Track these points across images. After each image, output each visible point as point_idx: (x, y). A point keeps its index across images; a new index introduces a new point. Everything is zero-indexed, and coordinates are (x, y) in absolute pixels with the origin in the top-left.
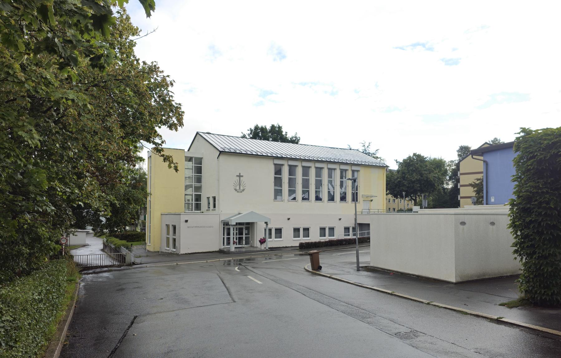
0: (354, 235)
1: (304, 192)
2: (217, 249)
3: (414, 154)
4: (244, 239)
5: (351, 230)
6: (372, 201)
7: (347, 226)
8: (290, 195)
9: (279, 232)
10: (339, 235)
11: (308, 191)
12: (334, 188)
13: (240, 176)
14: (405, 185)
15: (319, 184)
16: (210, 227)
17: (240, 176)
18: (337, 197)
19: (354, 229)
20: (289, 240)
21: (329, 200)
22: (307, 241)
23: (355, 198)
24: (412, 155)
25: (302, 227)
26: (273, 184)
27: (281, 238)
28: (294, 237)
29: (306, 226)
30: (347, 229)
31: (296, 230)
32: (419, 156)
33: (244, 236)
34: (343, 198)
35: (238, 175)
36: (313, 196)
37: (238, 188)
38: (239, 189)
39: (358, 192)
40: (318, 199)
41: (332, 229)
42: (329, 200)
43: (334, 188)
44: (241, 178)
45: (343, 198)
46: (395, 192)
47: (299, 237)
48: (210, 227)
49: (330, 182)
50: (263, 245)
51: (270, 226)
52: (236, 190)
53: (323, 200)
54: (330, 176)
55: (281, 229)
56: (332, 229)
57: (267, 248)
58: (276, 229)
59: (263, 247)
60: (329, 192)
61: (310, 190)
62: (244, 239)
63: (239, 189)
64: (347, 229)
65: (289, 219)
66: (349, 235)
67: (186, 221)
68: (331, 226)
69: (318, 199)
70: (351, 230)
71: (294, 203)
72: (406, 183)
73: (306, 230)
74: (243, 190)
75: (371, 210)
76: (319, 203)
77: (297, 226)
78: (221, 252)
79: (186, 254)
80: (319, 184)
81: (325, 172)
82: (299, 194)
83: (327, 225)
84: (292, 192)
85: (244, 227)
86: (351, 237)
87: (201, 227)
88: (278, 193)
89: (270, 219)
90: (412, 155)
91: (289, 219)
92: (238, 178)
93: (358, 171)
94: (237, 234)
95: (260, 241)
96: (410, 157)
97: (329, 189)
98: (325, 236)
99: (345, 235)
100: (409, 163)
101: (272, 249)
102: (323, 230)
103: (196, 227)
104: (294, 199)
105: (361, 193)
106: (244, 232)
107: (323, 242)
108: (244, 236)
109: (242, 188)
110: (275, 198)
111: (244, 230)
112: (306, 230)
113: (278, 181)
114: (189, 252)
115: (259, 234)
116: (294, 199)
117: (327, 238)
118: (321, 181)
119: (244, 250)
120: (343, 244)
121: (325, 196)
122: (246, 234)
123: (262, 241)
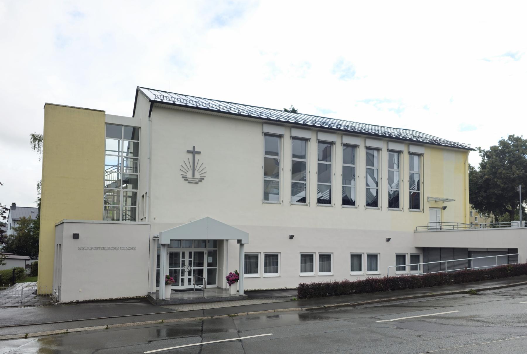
0: (413, 268)
1: (320, 189)
2: (142, 293)
3: (511, 137)
4: (205, 275)
5: (408, 259)
6: (445, 208)
7: (401, 251)
8: (294, 193)
9: (272, 261)
10: (387, 269)
11: (330, 188)
12: (377, 183)
13: (194, 152)
14: (499, 186)
15: (349, 174)
16: (129, 249)
17: (194, 152)
18: (384, 200)
19: (415, 258)
20: (290, 276)
21: (368, 205)
22: (374, 277)
23: (415, 203)
24: (497, 144)
25: (316, 252)
26: (262, 172)
27: (277, 272)
28: (302, 271)
29: (325, 251)
30: (400, 258)
31: (307, 260)
32: (518, 139)
33: (205, 268)
34: (394, 202)
35: (191, 149)
36: (337, 197)
37: (189, 175)
38: (193, 176)
39: (421, 192)
40: (347, 201)
41: (373, 258)
42: (368, 205)
43: (377, 183)
44: (197, 156)
45: (394, 202)
46: (480, 199)
47: (312, 271)
48: (129, 249)
49: (370, 172)
50: (233, 286)
51: (249, 249)
52: (185, 178)
53: (357, 204)
54: (370, 161)
55: (277, 255)
56: (373, 258)
57: (242, 293)
58: (267, 256)
59: (233, 290)
60: (368, 190)
61: (333, 184)
62: (205, 275)
63: (193, 176)
64: (400, 258)
65: (292, 237)
66: (404, 269)
67: (76, 236)
68: (373, 251)
69: (347, 201)
70: (408, 259)
71: (301, 207)
72: (499, 182)
73: (326, 258)
74: (201, 179)
75: (443, 224)
76: (348, 209)
77: (307, 251)
78: (148, 300)
79: (72, 303)
80: (349, 174)
81: (361, 155)
82: (312, 191)
83: (365, 250)
84: (297, 188)
85: (205, 250)
86: (408, 272)
87: (109, 249)
88: (270, 191)
89: (247, 235)
90: (497, 144)
91: (292, 237)
92: (190, 156)
93: (420, 155)
94: (183, 272)
95: (228, 278)
96: (502, 143)
97: (367, 185)
98: (360, 270)
99: (397, 269)
100: (502, 151)
101: (251, 294)
102: (356, 259)
103: (97, 248)
104: (303, 200)
105: (425, 195)
106: (206, 260)
107: (353, 284)
108: (205, 268)
109: (197, 176)
110: (266, 197)
111: (205, 257)
112: (326, 258)
113: (271, 169)
114: (80, 299)
115: (232, 262)
116: (303, 200)
117: (364, 274)
118: (353, 170)
119: (206, 295)
120: (399, 289)
121: (361, 199)
122: (209, 265)
123: (233, 279)
